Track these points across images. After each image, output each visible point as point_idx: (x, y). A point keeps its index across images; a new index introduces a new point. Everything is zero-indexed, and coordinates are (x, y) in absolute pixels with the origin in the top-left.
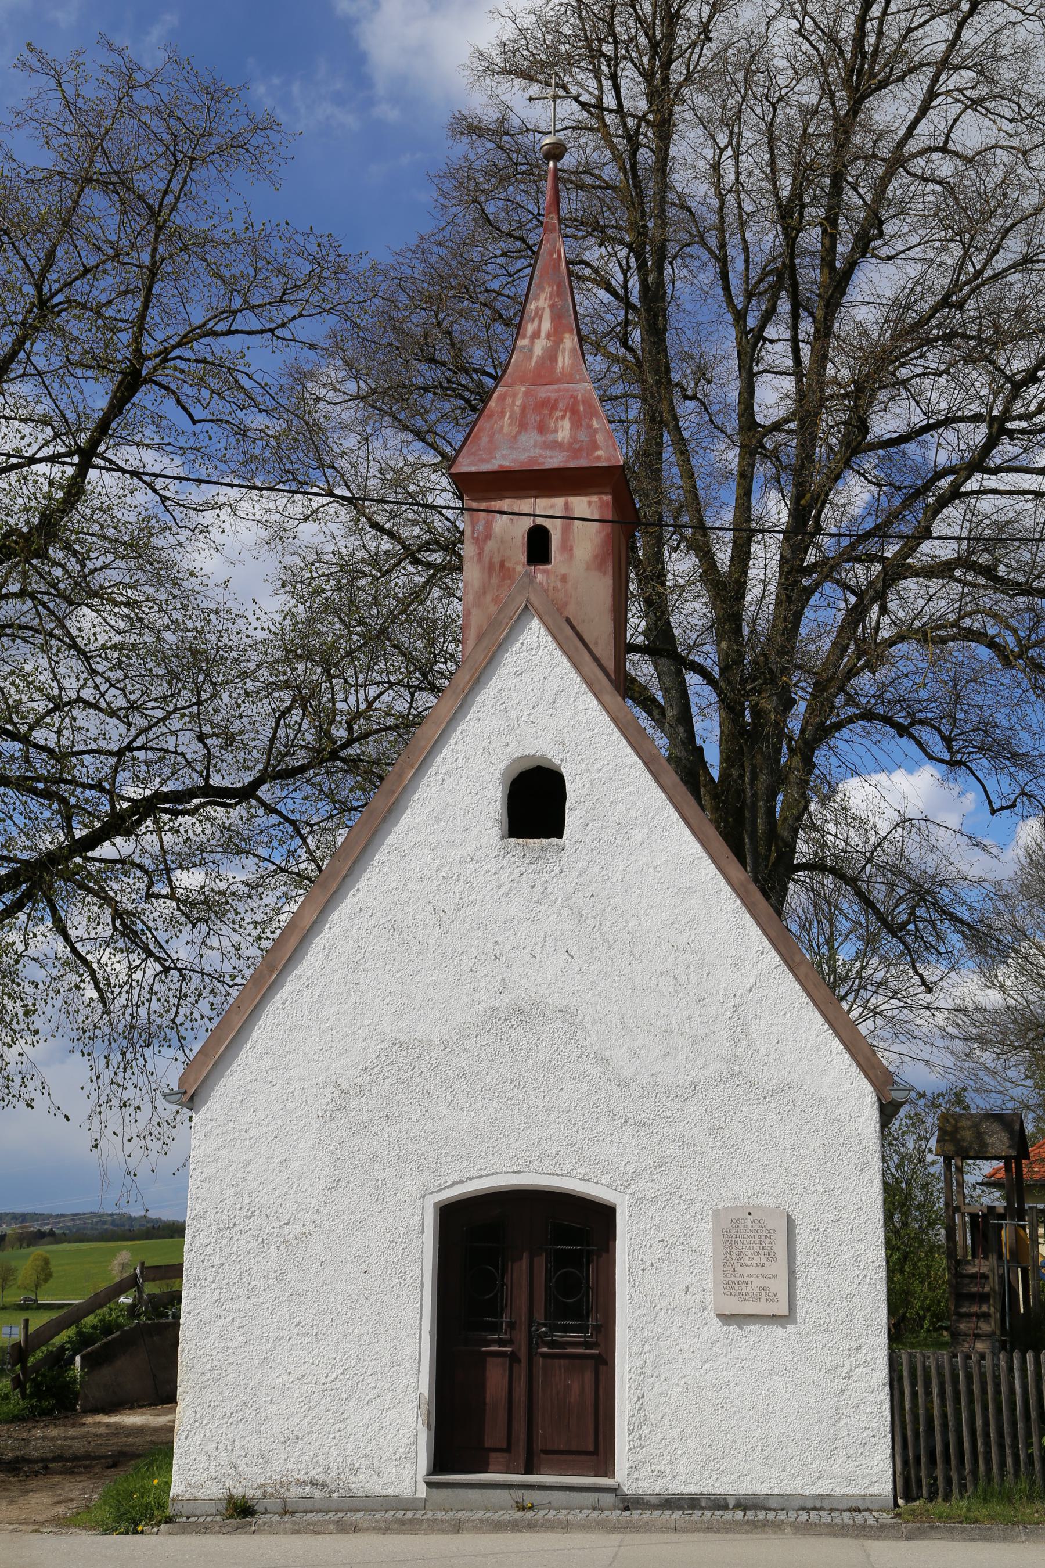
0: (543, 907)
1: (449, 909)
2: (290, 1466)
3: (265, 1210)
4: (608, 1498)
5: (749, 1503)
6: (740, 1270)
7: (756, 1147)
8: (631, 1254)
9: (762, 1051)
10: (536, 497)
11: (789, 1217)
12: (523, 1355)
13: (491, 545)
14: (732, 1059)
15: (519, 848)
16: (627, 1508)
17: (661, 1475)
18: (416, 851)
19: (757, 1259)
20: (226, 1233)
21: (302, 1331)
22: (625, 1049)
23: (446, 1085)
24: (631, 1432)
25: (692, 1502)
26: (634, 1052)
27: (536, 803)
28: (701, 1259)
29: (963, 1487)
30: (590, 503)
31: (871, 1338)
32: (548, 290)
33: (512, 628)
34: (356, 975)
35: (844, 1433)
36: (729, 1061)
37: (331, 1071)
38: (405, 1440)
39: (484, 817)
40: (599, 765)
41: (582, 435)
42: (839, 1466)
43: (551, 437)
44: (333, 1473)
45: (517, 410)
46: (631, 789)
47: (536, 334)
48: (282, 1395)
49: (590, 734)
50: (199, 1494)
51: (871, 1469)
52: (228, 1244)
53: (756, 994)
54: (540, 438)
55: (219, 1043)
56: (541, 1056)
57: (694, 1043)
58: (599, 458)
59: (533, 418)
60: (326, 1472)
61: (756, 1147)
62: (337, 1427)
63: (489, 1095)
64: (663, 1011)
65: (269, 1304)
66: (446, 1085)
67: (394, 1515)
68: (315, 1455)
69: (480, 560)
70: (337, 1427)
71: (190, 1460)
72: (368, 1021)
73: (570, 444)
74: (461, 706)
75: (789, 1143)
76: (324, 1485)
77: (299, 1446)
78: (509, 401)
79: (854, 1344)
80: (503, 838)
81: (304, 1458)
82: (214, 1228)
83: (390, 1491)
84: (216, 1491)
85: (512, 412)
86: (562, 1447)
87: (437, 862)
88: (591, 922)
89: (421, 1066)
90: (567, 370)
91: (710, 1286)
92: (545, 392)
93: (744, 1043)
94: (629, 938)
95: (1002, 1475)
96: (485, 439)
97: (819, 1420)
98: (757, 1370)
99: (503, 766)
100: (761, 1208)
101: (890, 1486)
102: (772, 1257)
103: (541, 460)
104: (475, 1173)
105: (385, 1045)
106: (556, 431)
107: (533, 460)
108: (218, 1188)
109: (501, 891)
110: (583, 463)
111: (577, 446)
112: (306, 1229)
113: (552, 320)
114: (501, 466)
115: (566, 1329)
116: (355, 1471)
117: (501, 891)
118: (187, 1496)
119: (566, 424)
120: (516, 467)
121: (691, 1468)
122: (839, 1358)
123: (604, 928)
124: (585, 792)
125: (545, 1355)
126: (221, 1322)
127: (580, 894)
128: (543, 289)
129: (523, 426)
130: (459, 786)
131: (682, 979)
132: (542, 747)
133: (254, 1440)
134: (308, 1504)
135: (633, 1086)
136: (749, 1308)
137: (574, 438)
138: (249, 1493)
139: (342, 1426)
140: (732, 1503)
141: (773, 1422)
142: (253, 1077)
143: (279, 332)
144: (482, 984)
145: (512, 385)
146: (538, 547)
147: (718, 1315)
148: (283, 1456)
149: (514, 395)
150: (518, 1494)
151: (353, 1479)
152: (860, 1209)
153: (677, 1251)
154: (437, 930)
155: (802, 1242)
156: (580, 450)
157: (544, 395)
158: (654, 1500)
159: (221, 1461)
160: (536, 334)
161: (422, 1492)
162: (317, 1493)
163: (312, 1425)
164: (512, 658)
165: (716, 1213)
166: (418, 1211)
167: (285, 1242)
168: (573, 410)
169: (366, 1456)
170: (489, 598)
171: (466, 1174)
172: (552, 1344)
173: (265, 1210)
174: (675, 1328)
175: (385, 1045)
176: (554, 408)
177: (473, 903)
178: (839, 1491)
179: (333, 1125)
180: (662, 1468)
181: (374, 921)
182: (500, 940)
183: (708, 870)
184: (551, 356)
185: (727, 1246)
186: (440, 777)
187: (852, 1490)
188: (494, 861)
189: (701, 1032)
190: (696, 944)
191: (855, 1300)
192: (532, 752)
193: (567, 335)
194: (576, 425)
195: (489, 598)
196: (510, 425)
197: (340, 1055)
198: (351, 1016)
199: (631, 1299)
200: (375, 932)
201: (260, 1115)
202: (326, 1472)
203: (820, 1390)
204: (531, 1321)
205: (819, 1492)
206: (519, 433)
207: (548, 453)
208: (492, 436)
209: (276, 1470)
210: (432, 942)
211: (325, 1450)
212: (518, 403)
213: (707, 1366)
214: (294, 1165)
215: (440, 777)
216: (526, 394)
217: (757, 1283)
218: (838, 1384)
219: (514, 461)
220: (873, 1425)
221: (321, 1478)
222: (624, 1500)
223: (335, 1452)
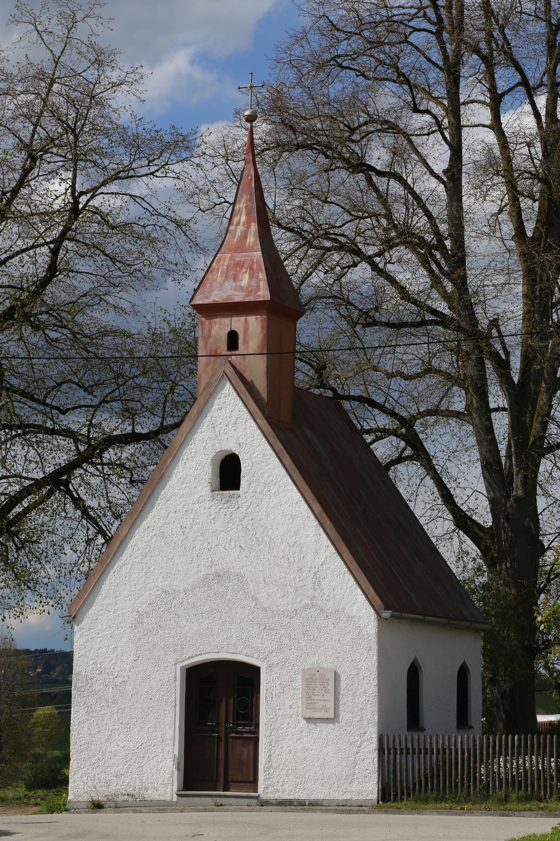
0: (230, 525)
1: (188, 526)
2: (119, 787)
3: (107, 671)
4: (254, 801)
5: (315, 803)
6: (313, 697)
7: (322, 640)
8: (267, 690)
9: (326, 594)
10: (231, 316)
11: (335, 673)
12: (223, 737)
13: (210, 340)
14: (313, 598)
15: (219, 496)
16: (262, 806)
17: (278, 791)
18: (173, 498)
19: (321, 692)
20: (90, 681)
21: (123, 726)
22: (265, 594)
23: (186, 611)
24: (265, 772)
25: (290, 803)
26: (269, 595)
27: (229, 472)
28: (297, 692)
29: (409, 795)
30: (256, 318)
31: (371, 729)
32: (245, 198)
33: (216, 386)
34: (146, 559)
35: (357, 772)
36: (311, 599)
37: (135, 605)
38: (168, 776)
39: (203, 481)
40: (256, 455)
41: (253, 283)
42: (355, 787)
43: (239, 284)
44: (137, 790)
45: (225, 268)
46: (270, 466)
47: (238, 223)
48: (115, 755)
49: (252, 439)
50: (80, 799)
51: (369, 788)
52: (91, 687)
53: (325, 567)
54: (234, 285)
55: (85, 592)
56: (228, 597)
57: (296, 591)
58: (259, 296)
59: (232, 273)
60: (134, 790)
61: (322, 640)
62: (139, 769)
63: (205, 616)
64: (283, 575)
65: (109, 714)
66: (186, 611)
67: (162, 807)
68: (130, 782)
69: (205, 348)
70: (139, 769)
71: (76, 784)
72: (151, 581)
73: (247, 287)
74: (193, 426)
75: (337, 638)
76: (133, 796)
77: (123, 778)
78: (222, 262)
79: (363, 731)
80: (213, 491)
81: (125, 783)
82: (84, 679)
83: (161, 798)
84: (86, 798)
85: (223, 269)
86: (239, 779)
87: (183, 504)
88: (251, 532)
89: (176, 602)
90: (251, 243)
91: (300, 705)
92: (240, 257)
93: (319, 590)
94: (268, 540)
95: (426, 790)
96: (208, 285)
97: (347, 766)
98: (321, 741)
99: (212, 455)
100: (323, 668)
101: (376, 796)
102: (327, 691)
103: (233, 297)
104: (199, 653)
105: (159, 592)
106: (241, 280)
107: (229, 297)
108: (86, 660)
109: (211, 518)
110: (251, 299)
111: (250, 289)
112: (125, 679)
113: (246, 215)
114: (214, 301)
115: (244, 725)
116: (147, 790)
117: (211, 518)
118: (75, 800)
119: (247, 276)
120: (221, 301)
121: (291, 788)
122: (356, 738)
123: (257, 535)
124: (249, 468)
125: (233, 738)
126: (88, 722)
127: (247, 519)
128: (242, 197)
129: (226, 277)
130: (194, 463)
131: (292, 560)
132: (232, 447)
133: (103, 775)
134: (126, 804)
135: (269, 611)
136: (317, 715)
137: (249, 284)
138: (100, 799)
139: (141, 769)
140: (307, 803)
141: (327, 767)
142: (101, 608)
143: (156, 174)
144: (202, 563)
145: (225, 253)
146: (233, 340)
147: (304, 718)
148: (116, 783)
149: (225, 259)
150: (215, 799)
151: (146, 793)
152: (367, 669)
153: (287, 689)
154: (182, 537)
155: (343, 684)
156: (251, 291)
157: (238, 259)
158: (274, 802)
159: (89, 784)
160: (238, 223)
161: (175, 798)
162: (130, 799)
163: (128, 769)
164: (218, 402)
165: (303, 671)
166: (173, 670)
167: (115, 685)
168: (251, 268)
169: (151, 783)
170: (210, 368)
171: (195, 653)
172: (236, 732)
173: (107, 671)
174: (285, 724)
175: (159, 592)
176: (242, 267)
177: (199, 523)
178: (355, 798)
179: (136, 631)
180: (278, 788)
181: (154, 532)
182: (210, 541)
183: (304, 506)
184: (244, 236)
185: (308, 686)
186: (183, 462)
187: (360, 798)
188: (208, 503)
189: (300, 585)
190: (298, 542)
191: (364, 711)
192: (226, 448)
193: (253, 224)
194: (251, 277)
195: (210, 368)
196: (221, 277)
197: (139, 597)
198: (144, 578)
199: (266, 711)
200: (155, 538)
201: (104, 626)
202: (134, 790)
203: (347, 753)
204: (227, 722)
205: (346, 798)
206: (224, 281)
207: (237, 293)
208: (211, 283)
209: (113, 789)
210: (180, 543)
211: (134, 780)
212: (226, 264)
213: (299, 742)
214: (119, 649)
215: (183, 462)
216: (231, 258)
217: (321, 703)
218: (355, 750)
219: (220, 298)
220: (370, 768)
221: (132, 792)
222: (261, 802)
223: (138, 781)
